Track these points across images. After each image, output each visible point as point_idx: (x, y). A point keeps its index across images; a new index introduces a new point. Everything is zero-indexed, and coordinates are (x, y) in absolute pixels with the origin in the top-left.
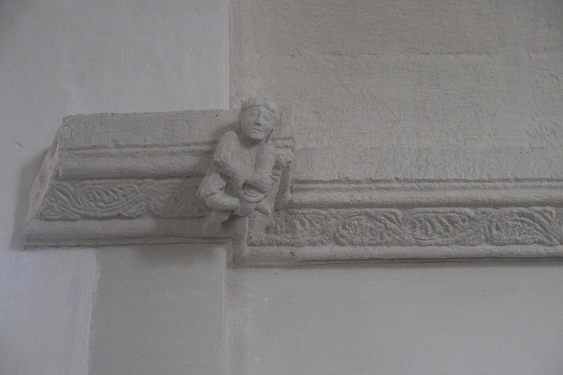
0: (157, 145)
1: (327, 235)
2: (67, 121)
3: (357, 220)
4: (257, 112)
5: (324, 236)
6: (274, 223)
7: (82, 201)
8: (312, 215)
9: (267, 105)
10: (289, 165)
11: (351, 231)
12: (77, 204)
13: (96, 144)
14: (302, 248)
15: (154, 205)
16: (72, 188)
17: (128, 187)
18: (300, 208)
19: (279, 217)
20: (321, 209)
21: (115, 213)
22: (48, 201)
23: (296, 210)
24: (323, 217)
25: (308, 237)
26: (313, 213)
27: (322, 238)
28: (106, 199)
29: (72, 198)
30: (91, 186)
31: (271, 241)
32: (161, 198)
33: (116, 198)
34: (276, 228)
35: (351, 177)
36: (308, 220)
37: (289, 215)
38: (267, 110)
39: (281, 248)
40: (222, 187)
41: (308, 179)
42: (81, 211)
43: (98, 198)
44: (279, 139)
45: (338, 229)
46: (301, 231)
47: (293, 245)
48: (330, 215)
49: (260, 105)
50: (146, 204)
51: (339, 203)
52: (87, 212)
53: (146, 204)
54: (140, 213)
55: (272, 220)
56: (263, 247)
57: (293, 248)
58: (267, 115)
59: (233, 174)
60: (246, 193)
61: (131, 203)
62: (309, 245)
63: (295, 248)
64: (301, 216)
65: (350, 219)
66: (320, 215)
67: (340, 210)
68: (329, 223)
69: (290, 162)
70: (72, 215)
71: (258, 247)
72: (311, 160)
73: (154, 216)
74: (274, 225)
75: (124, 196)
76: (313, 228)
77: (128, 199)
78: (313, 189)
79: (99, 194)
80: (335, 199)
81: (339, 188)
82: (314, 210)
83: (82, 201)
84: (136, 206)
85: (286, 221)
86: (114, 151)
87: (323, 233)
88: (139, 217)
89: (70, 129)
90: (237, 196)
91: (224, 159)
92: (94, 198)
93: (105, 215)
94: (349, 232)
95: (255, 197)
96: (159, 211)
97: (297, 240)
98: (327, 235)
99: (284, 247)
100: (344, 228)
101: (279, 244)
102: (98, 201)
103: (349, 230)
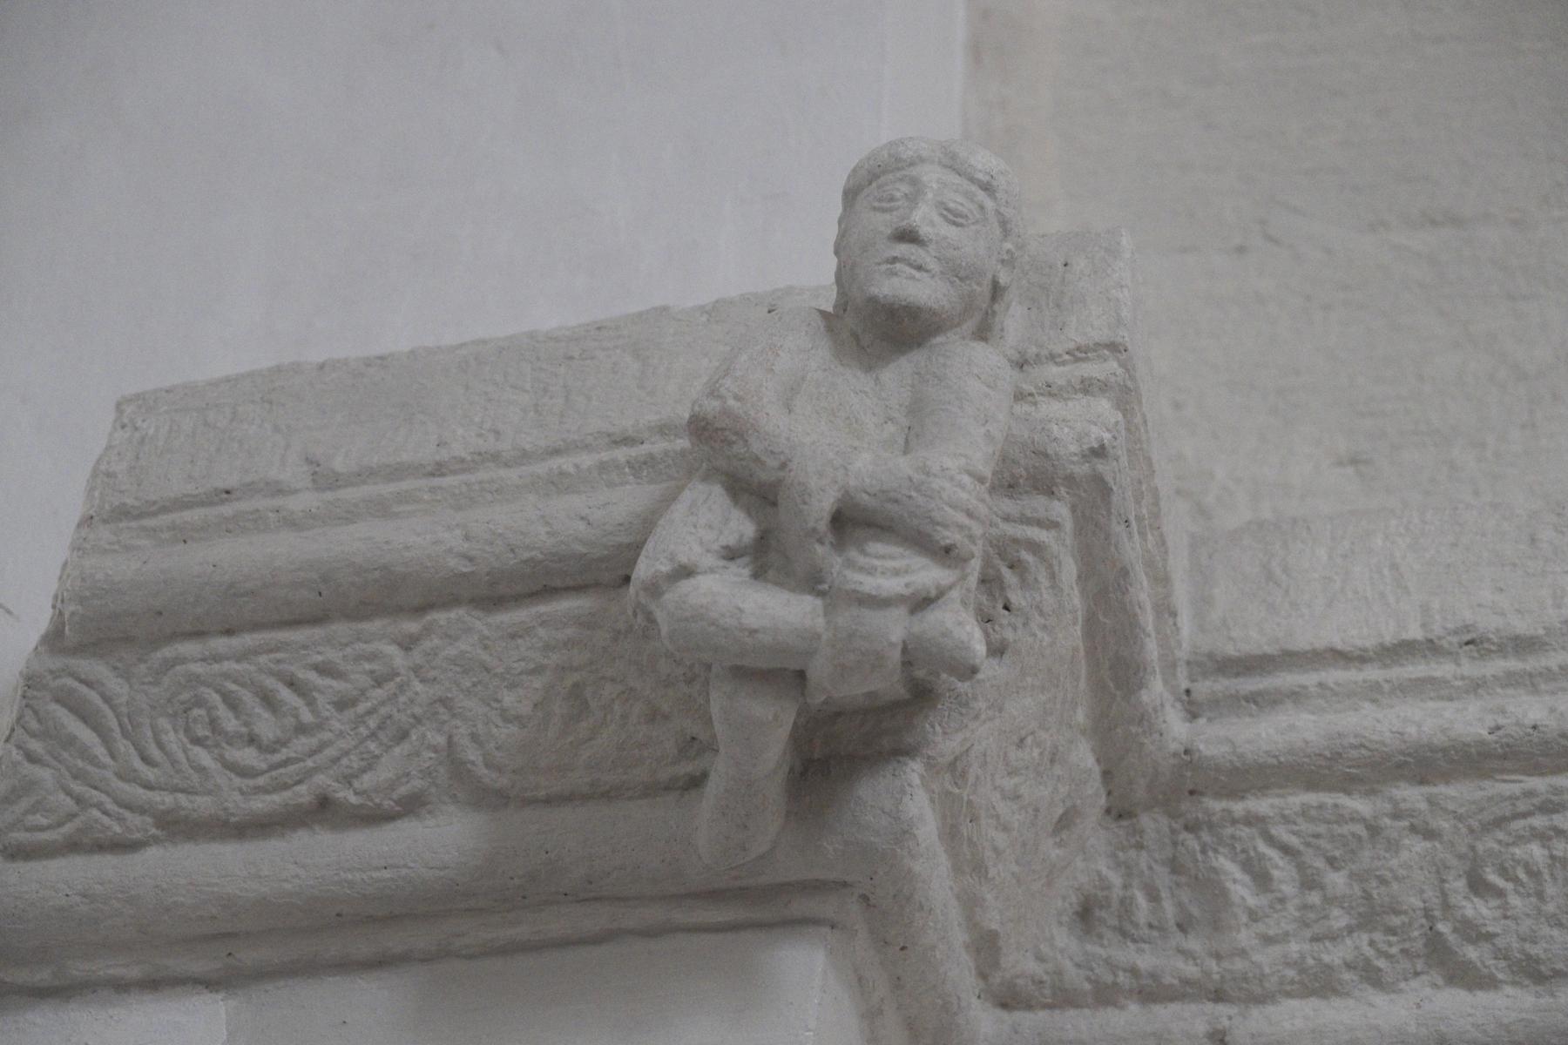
0: (495, 457)
1: (1392, 931)
2: (129, 409)
3: (1542, 837)
4: (905, 188)
5: (1378, 936)
6: (1116, 879)
7: (161, 746)
8: (1304, 826)
9: (954, 157)
10: (1101, 467)
11: (1515, 901)
12: (137, 763)
13: (232, 481)
14: (1270, 1009)
15: (474, 737)
16: (116, 685)
17: (358, 658)
18: (1235, 794)
19: (1140, 846)
20: (1348, 793)
21: (303, 794)
22: (17, 755)
23: (1216, 806)
24: (1360, 829)
25: (1294, 947)
26: (1304, 812)
27: (1369, 952)
28: (267, 727)
29: (117, 734)
30: (197, 668)
31: (1109, 979)
32: (508, 699)
33: (307, 717)
34: (1127, 905)
35: (1488, 623)
36: (1286, 850)
37: (1184, 835)
38: (957, 180)
39: (1164, 1013)
40: (730, 539)
41: (1268, 650)
42: (156, 797)
43: (231, 723)
44: (1052, 357)
45: (1444, 895)
46: (1254, 916)
47: (1219, 996)
48: (1396, 816)
49: (922, 160)
50: (441, 740)
51: (1433, 749)
52: (182, 799)
53: (441, 740)
54: (418, 783)
55: (1102, 865)
56: (1072, 1012)
57: (1222, 1009)
58: (956, 200)
59: (783, 466)
60: (850, 564)
61: (373, 735)
62: (1307, 992)
63: (1232, 1010)
64: (1244, 832)
65: (1500, 835)
66: (1341, 819)
67: (1441, 789)
68: (1394, 862)
69: (1099, 452)
70: (120, 820)
71: (1043, 1015)
72: (1286, 570)
73: (488, 799)
74: (1117, 893)
75: (342, 704)
76: (1314, 898)
77: (360, 720)
78: (1297, 696)
79: (233, 704)
80: (1412, 730)
81: (1431, 680)
82: (1312, 798)
83: (161, 746)
84: (397, 750)
85: (1175, 867)
86: (304, 502)
87: (1369, 917)
88: (412, 806)
89: (137, 435)
90: (813, 582)
91: (737, 398)
92: (213, 723)
93: (260, 804)
94: (1505, 906)
95: (897, 573)
96: (500, 769)
97: (1239, 965)
98: (1392, 931)
99: (1174, 1007)
100: (1478, 886)
101: (1151, 992)
102: (231, 739)
103: (1500, 893)
